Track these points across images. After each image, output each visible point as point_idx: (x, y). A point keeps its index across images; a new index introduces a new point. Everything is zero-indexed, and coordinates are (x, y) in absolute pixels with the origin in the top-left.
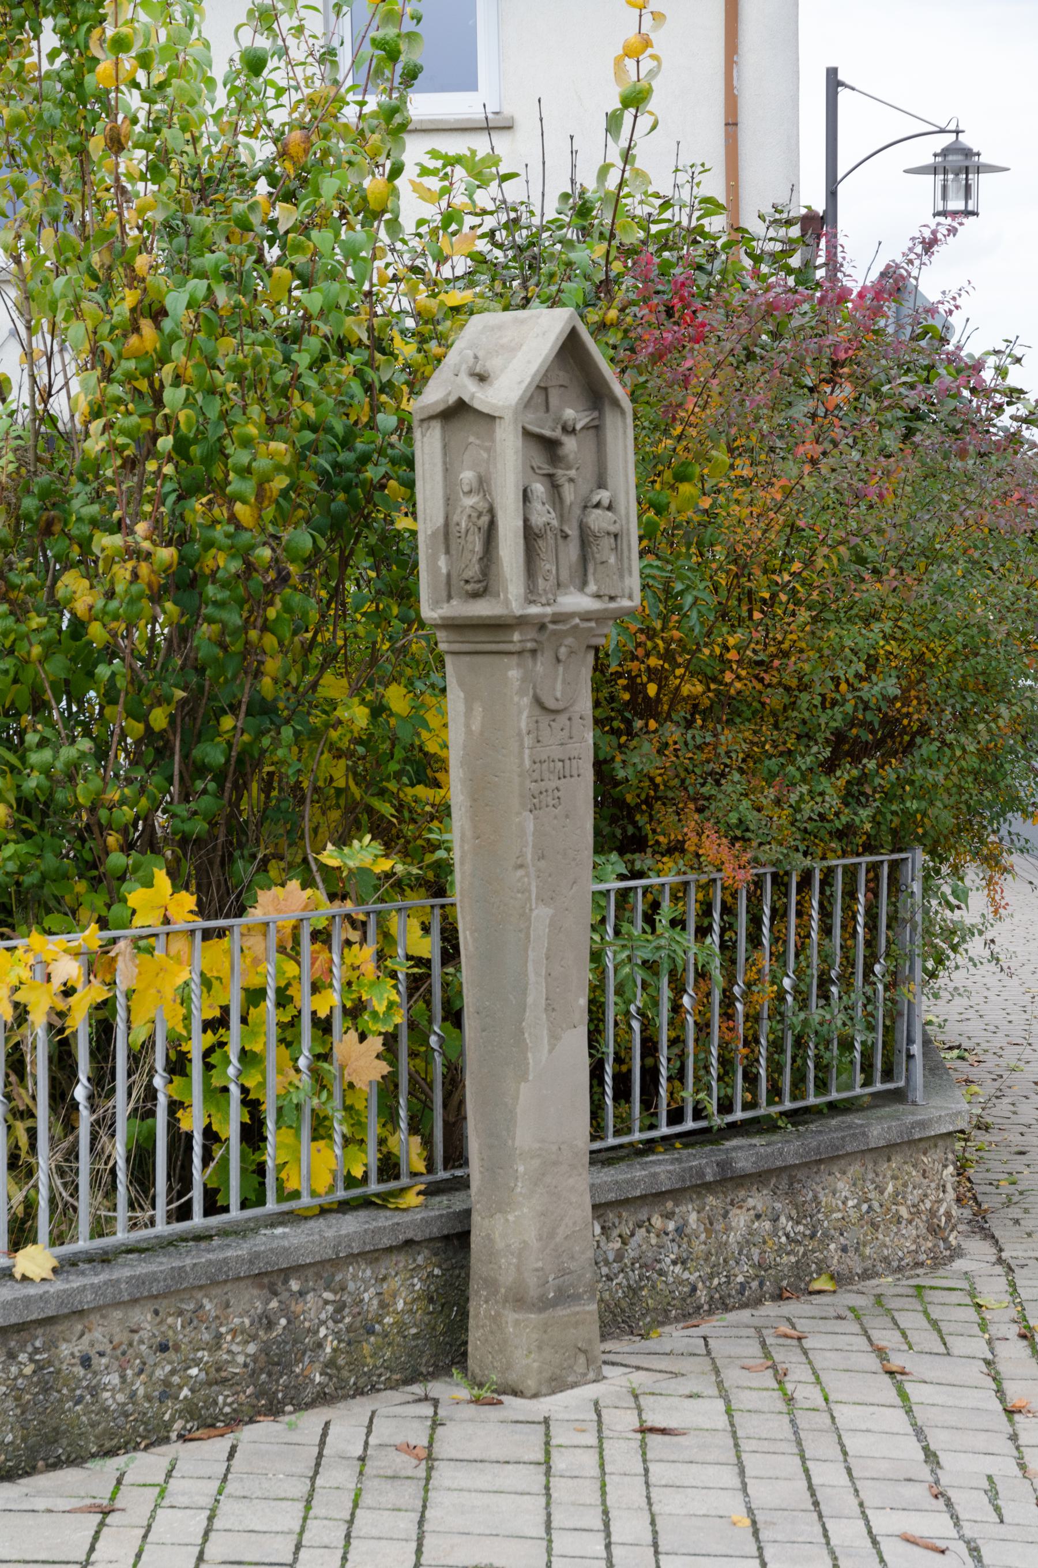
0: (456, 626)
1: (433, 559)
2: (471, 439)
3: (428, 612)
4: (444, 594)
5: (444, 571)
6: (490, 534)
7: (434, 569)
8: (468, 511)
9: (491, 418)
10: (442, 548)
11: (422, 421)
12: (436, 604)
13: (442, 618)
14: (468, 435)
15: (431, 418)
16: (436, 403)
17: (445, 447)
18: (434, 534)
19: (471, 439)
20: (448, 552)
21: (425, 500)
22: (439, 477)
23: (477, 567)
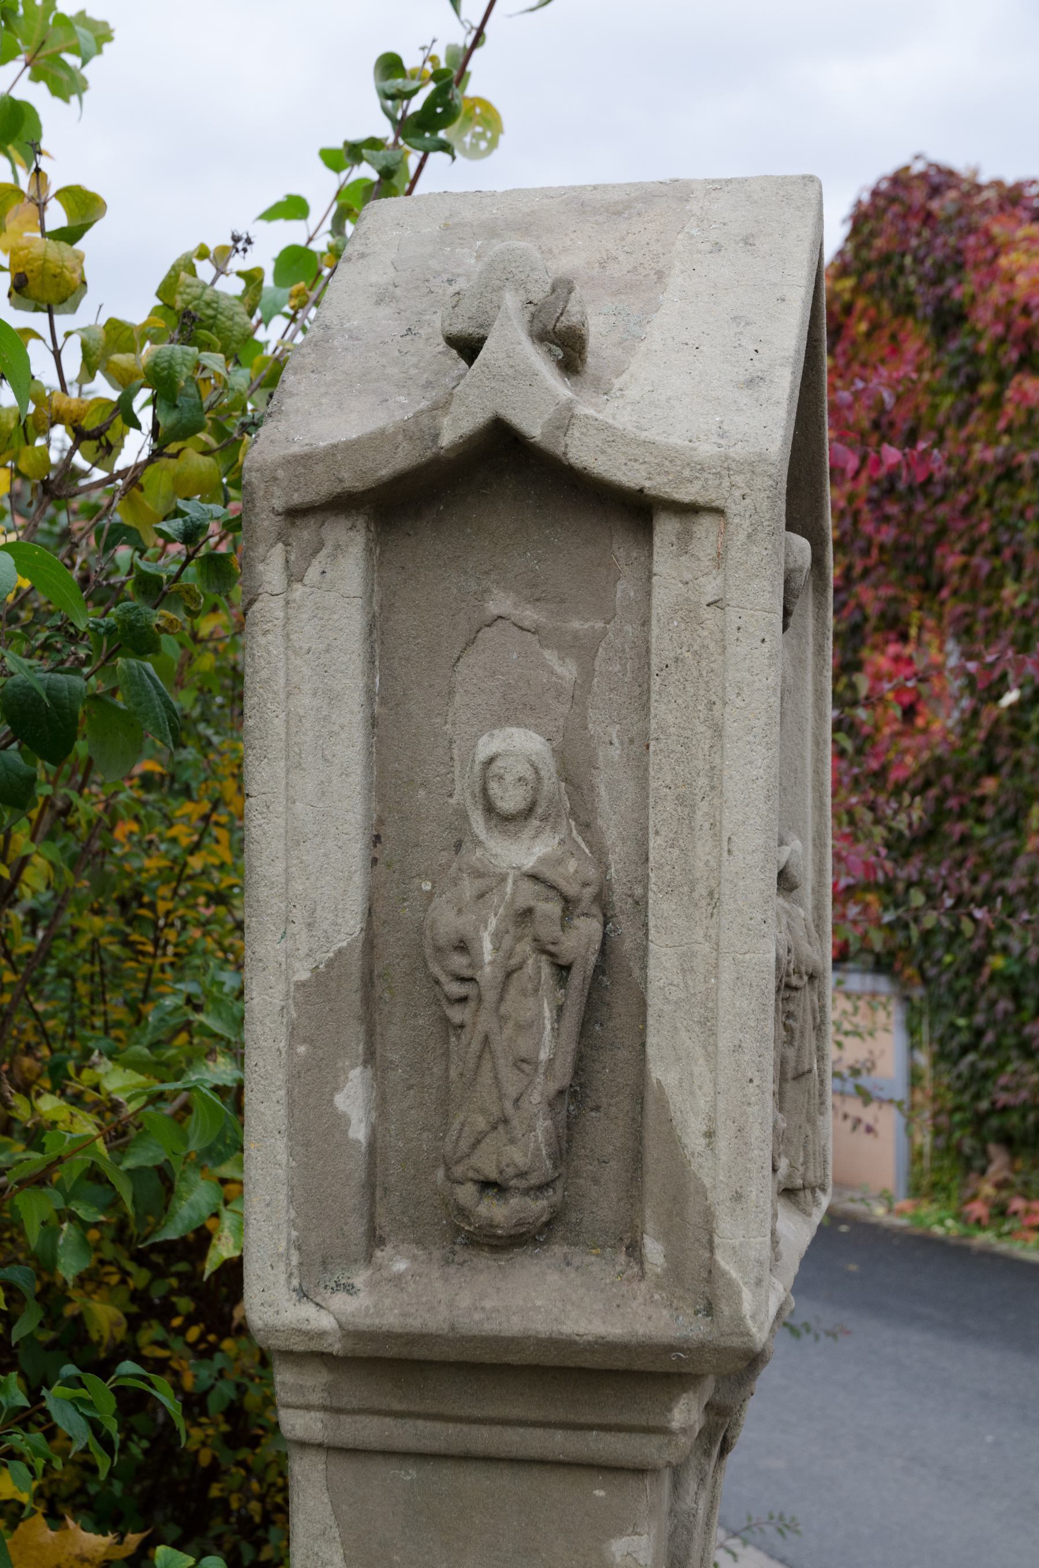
0: (387, 1365)
1: (311, 1087)
2: (500, 603)
3: (272, 1303)
4: (356, 1228)
5: (359, 1132)
6: (603, 994)
7: (312, 1123)
8: (515, 893)
9: (636, 511)
10: (354, 1036)
11: (295, 514)
12: (314, 1274)
13: (350, 1334)
14: (504, 584)
15: (341, 504)
16: (377, 440)
17: (378, 630)
18: (320, 985)
19: (500, 603)
20: (370, 1058)
21: (294, 840)
22: (350, 747)
23: (543, 1125)
